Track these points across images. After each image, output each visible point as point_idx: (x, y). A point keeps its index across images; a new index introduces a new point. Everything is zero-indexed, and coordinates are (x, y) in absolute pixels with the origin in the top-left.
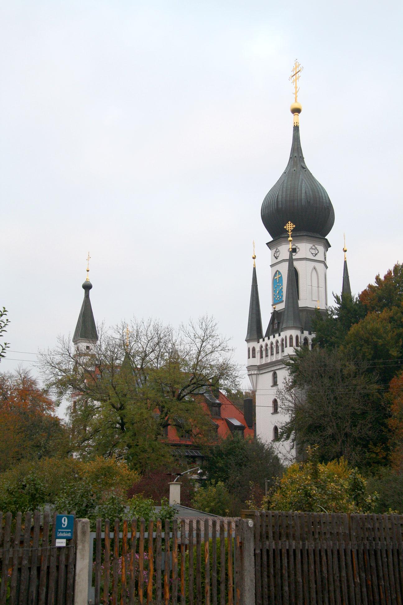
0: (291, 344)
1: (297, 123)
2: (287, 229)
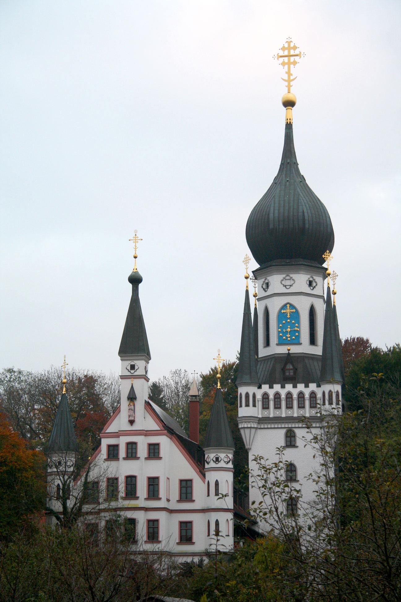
1: (290, 119)
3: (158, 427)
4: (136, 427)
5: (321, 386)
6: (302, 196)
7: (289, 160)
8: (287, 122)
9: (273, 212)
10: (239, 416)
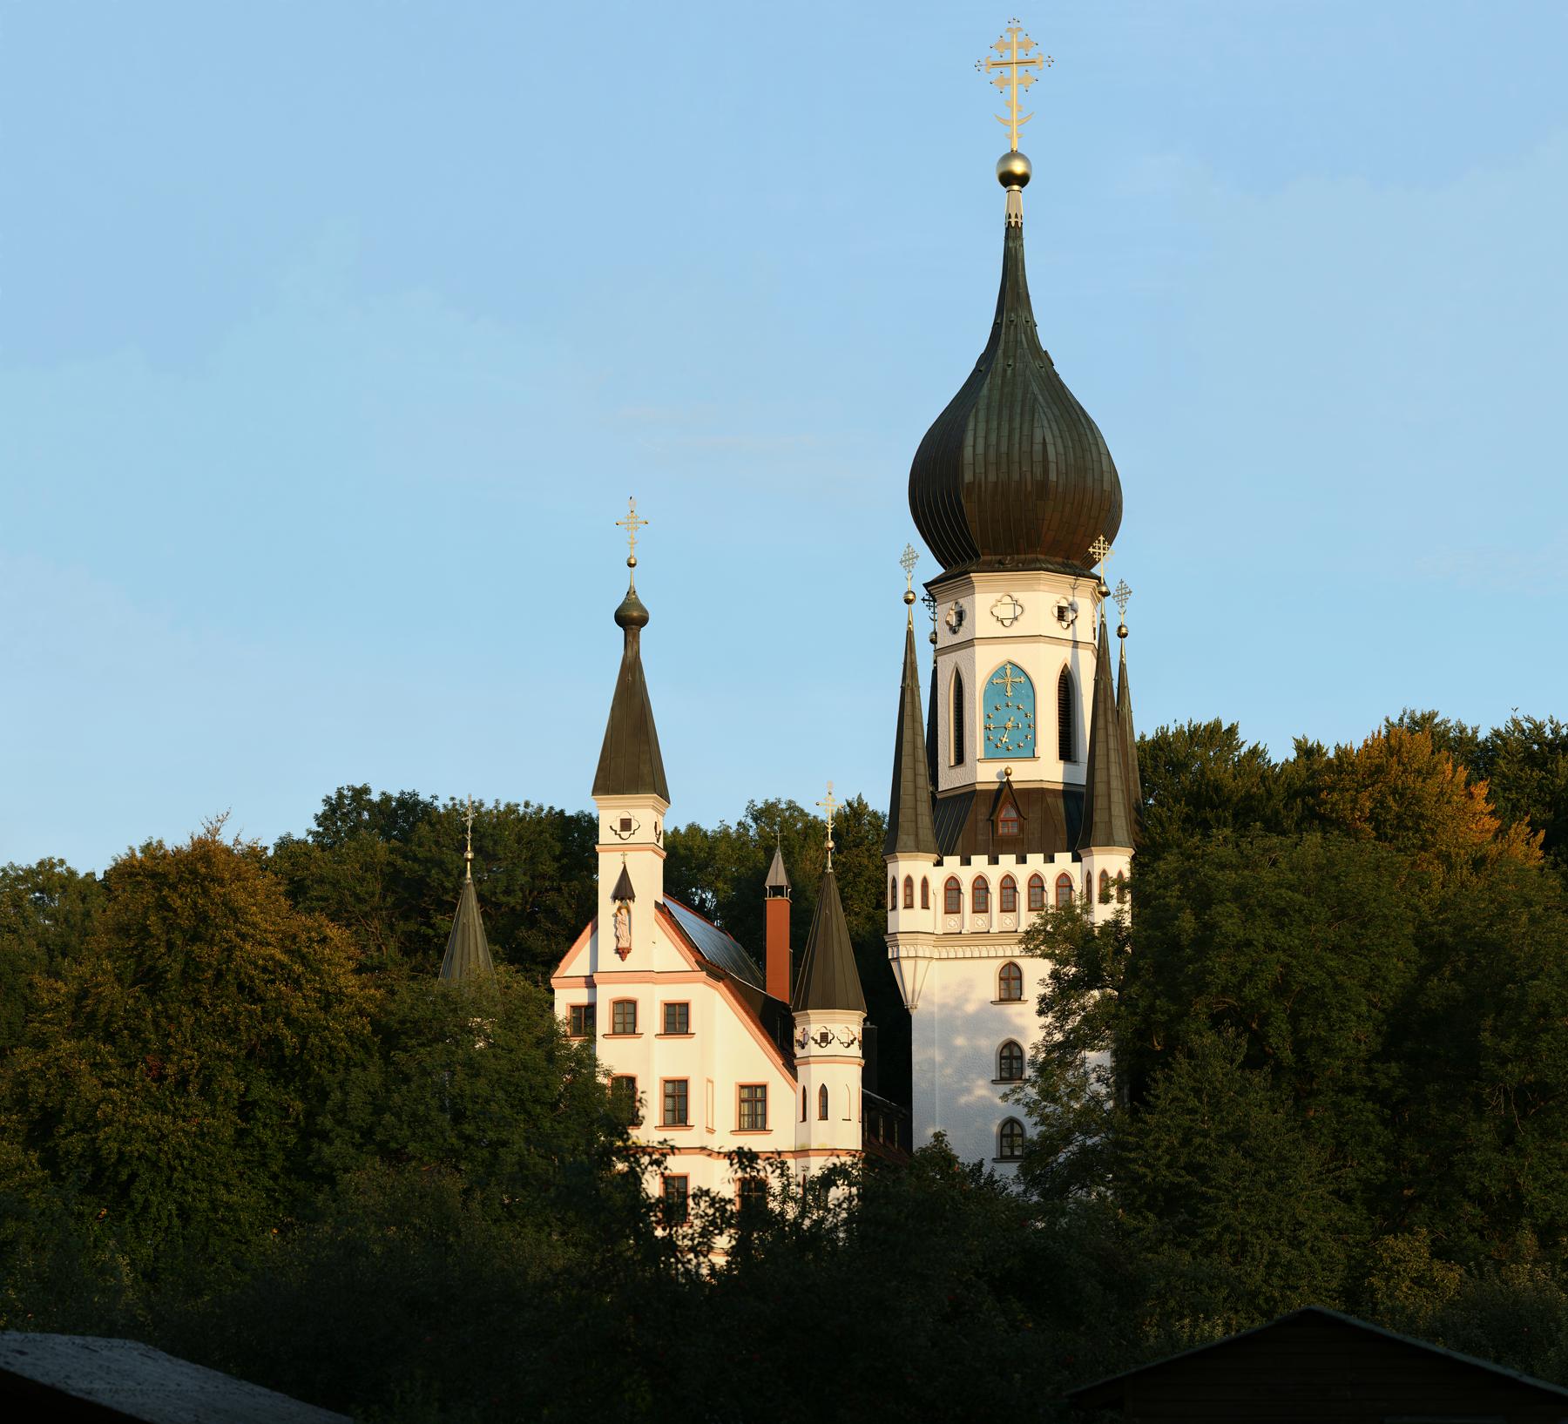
3: (688, 966)
4: (631, 963)
5: (1083, 859)
6: (1044, 404)
7: (1013, 315)
9: (972, 443)
10: (889, 932)
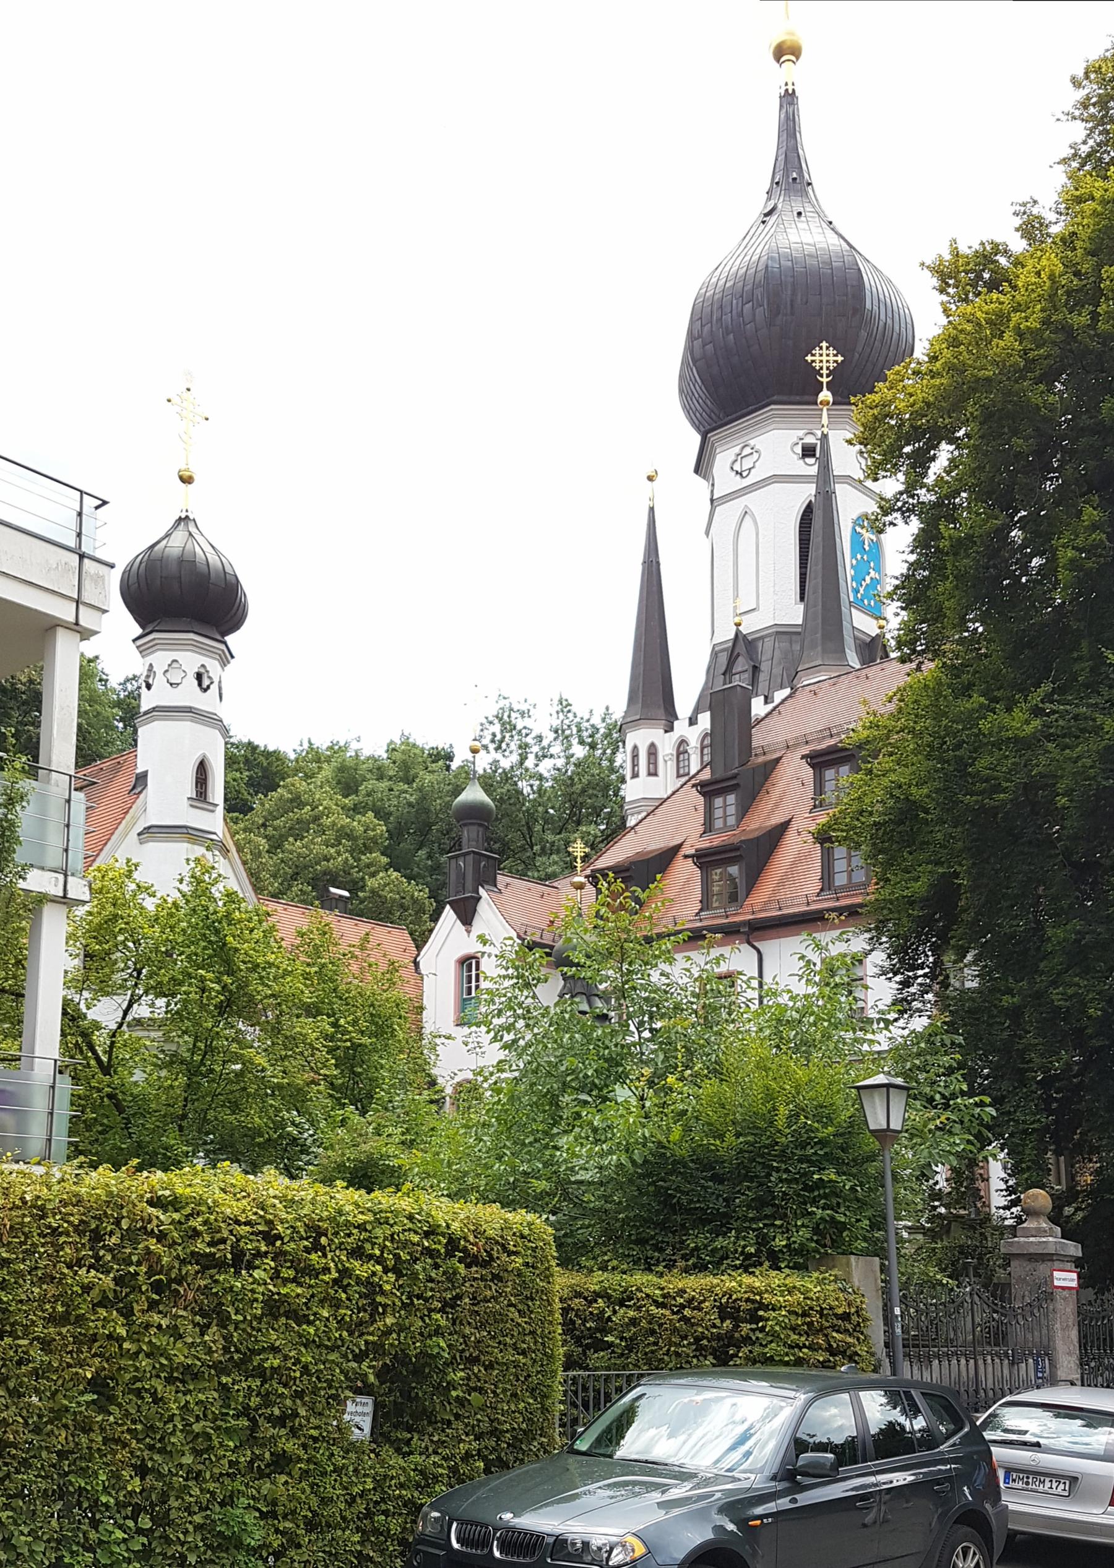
0: (652, 771)
2: (817, 365)
8: (787, 90)
